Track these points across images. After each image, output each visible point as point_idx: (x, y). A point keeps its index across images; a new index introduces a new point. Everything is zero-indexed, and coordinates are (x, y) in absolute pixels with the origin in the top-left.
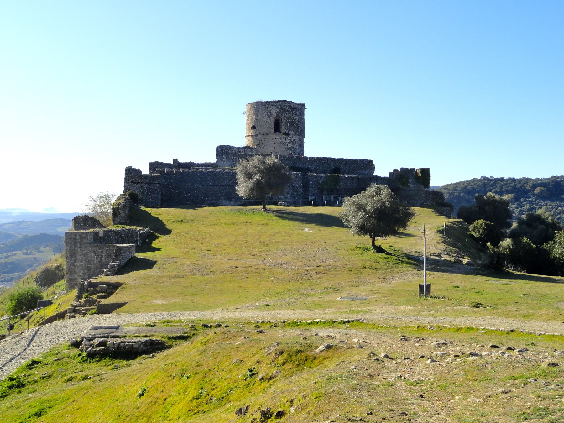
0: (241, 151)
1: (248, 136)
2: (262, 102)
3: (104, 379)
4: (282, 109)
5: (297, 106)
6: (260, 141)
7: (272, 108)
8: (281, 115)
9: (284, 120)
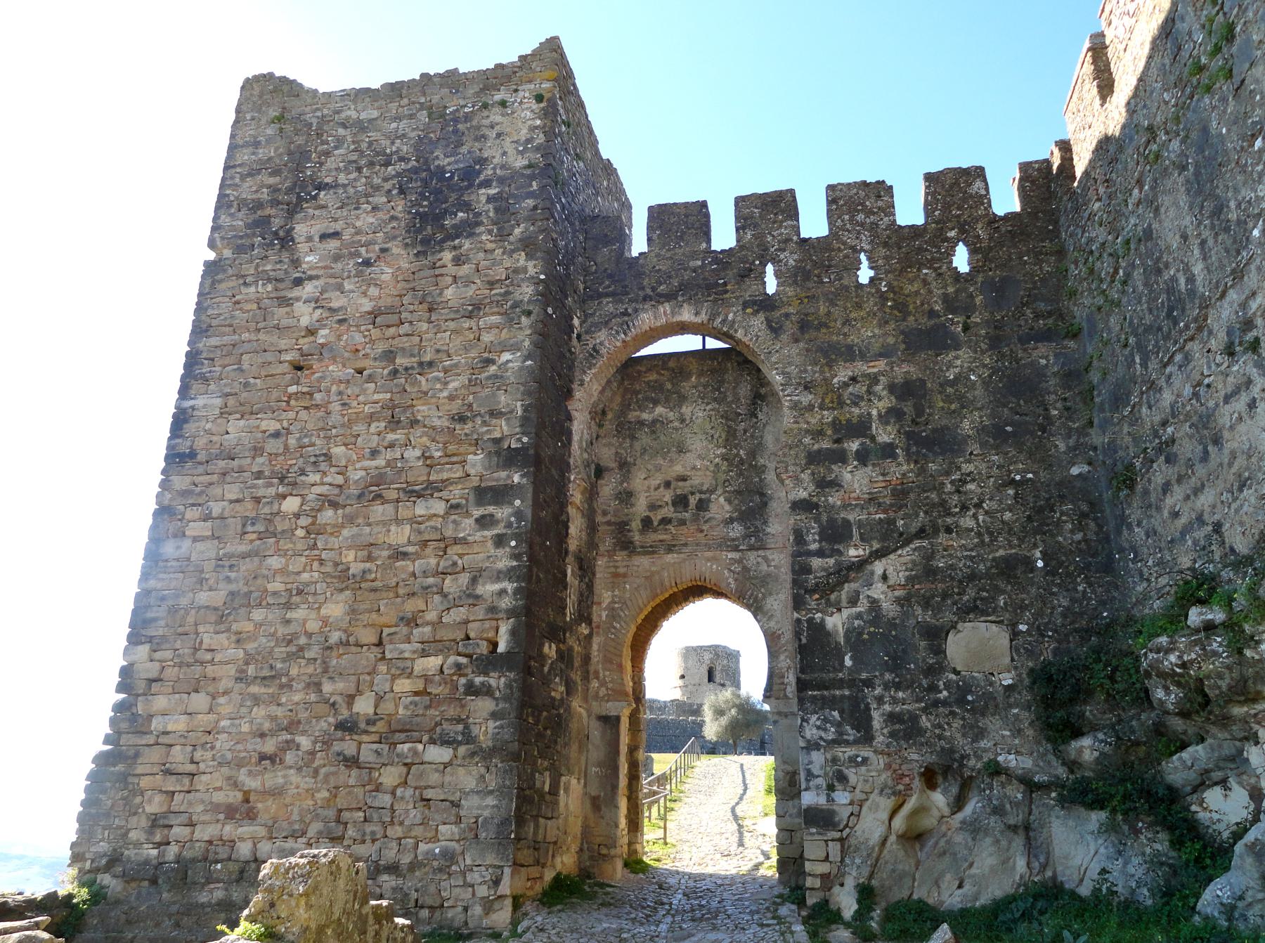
4: (717, 654)
6: (691, 693)
9: (719, 668)
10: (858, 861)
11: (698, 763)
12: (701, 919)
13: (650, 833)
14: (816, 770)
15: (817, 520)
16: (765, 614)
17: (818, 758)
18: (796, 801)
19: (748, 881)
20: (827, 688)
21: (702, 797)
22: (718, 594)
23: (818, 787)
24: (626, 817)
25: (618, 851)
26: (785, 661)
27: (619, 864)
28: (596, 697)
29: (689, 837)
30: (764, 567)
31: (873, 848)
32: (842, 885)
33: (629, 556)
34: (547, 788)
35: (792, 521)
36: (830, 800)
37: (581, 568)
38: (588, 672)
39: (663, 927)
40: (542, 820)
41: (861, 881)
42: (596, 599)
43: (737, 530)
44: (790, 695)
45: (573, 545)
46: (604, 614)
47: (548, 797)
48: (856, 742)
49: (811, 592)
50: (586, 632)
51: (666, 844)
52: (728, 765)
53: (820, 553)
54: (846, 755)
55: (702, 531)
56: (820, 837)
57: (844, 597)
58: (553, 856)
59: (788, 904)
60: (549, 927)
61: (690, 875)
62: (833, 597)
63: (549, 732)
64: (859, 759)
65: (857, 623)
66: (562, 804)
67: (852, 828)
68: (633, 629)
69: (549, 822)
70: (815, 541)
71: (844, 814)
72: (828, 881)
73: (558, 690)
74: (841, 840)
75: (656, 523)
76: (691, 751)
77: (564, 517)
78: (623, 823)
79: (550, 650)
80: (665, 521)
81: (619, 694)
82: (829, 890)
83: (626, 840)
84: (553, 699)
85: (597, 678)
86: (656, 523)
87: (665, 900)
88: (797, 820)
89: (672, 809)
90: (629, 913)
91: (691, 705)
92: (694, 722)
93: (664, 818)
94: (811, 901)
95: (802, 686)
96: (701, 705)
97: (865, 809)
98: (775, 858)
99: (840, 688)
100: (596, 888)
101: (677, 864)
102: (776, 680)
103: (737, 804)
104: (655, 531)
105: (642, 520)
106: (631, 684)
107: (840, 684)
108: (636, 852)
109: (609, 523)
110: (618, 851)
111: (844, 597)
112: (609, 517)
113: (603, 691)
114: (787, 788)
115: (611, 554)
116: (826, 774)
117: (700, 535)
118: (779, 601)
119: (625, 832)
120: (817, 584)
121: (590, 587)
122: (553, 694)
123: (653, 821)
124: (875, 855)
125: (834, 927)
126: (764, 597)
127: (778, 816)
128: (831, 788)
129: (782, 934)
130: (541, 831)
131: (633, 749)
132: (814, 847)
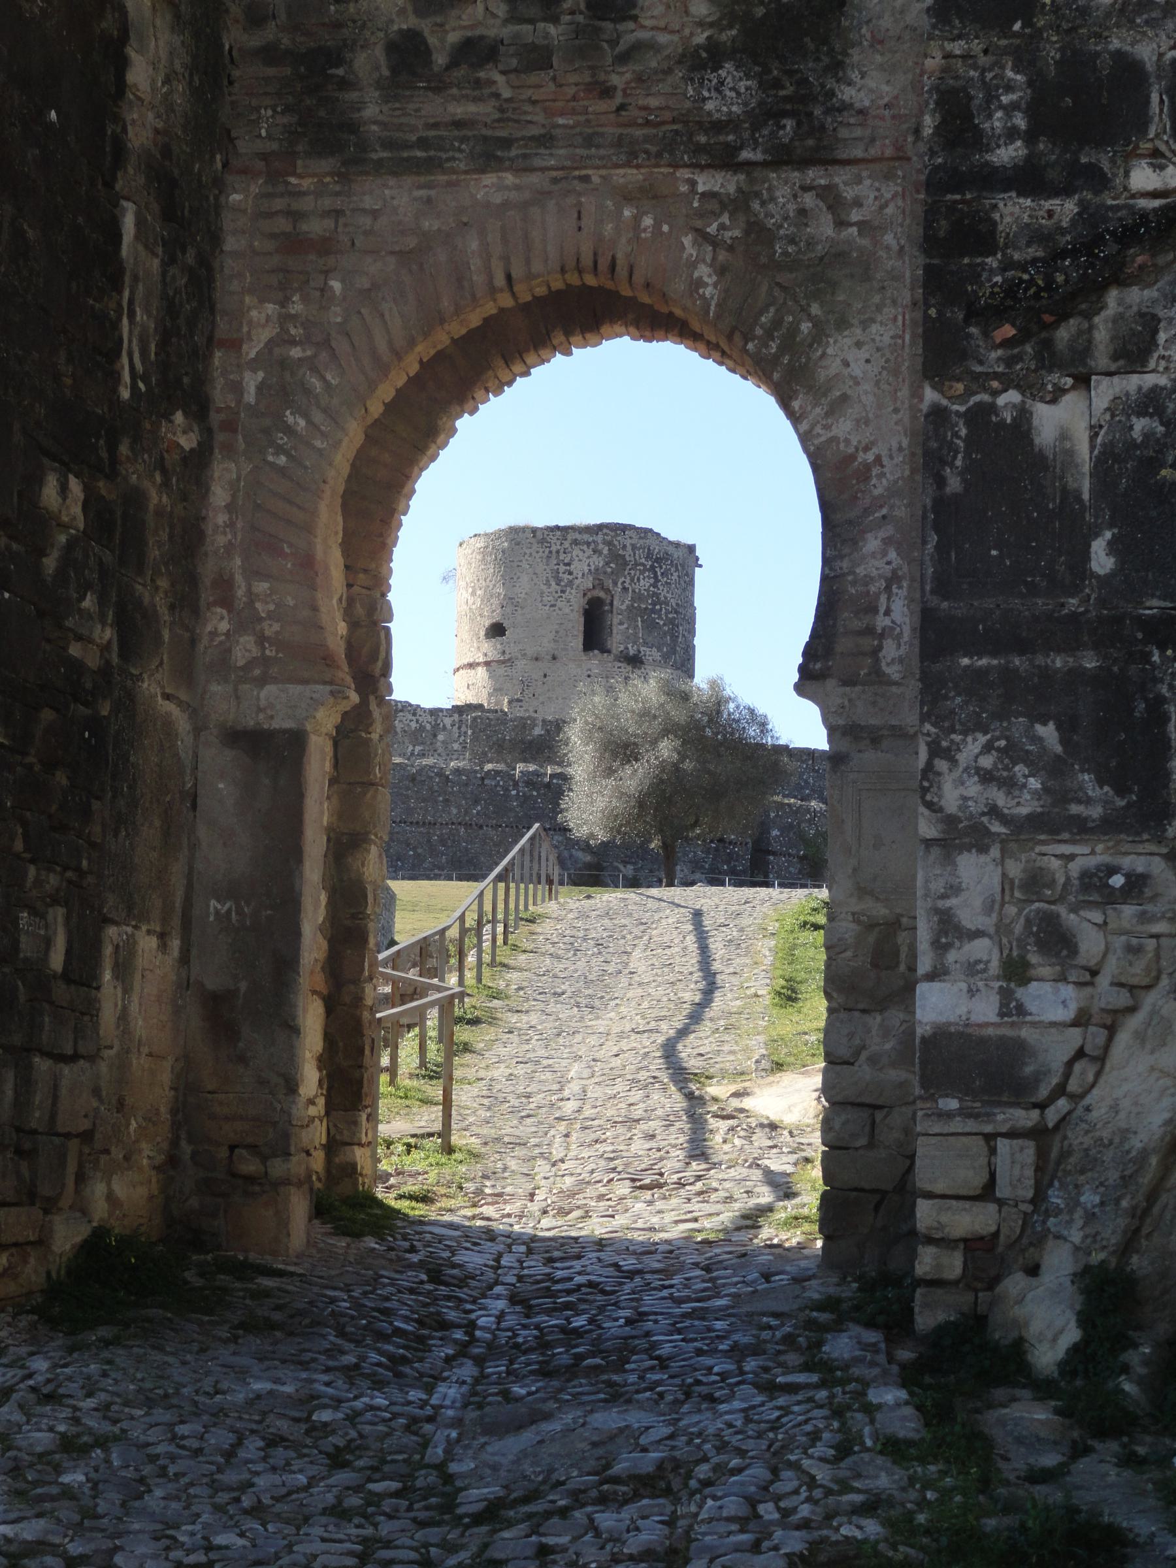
0: (448, 721)
1: (471, 666)
2: (534, 531)
3: (622, 1395)
4: (617, 558)
5: (671, 550)
6: (525, 684)
7: (576, 551)
8: (609, 583)
9: (621, 604)
10: (1089, 1198)
11: (552, 907)
12: (573, 1370)
13: (397, 1119)
14: (970, 913)
15: (1025, 58)
16: (818, 392)
17: (978, 875)
18: (895, 1016)
19: (715, 1272)
20: (1024, 647)
21: (565, 1012)
22: (655, 322)
23: (972, 968)
24: (323, 1062)
25: (295, 1165)
26: (877, 557)
27: (299, 1207)
28: (223, 665)
29: (526, 1129)
30: (824, 228)
31: (1144, 1154)
32: (1033, 1270)
33: (343, 177)
34: (57, 960)
35: (933, 63)
36: (1011, 1008)
37: (169, 214)
38: (193, 580)
39: (449, 1393)
40: (42, 1064)
41: (1097, 1257)
42: (223, 328)
43: (730, 93)
44: (893, 671)
45: (141, 128)
46: (251, 382)
47: (61, 992)
48: (1110, 826)
49: (987, 315)
50: (188, 442)
51: (449, 1149)
52: (656, 922)
53: (1028, 180)
54: (1075, 868)
55: (607, 92)
56: (971, 1126)
57: (1102, 335)
58: (81, 1178)
59: (856, 1329)
60: (73, 1388)
61: (531, 1243)
62: (1064, 334)
63: (61, 778)
64: (1117, 881)
65: (1140, 425)
66: (108, 1015)
67: (1076, 1098)
68: (353, 435)
69: (66, 1070)
70: (1012, 134)
71: (1056, 1051)
72: (987, 1259)
73: (95, 639)
74: (1039, 1134)
75: (440, 59)
76: (527, 873)
77: (108, 24)
78: (310, 1079)
79: (63, 498)
80: (476, 52)
81: (304, 659)
82: (996, 1280)
83: (318, 1134)
84: (77, 666)
85: (227, 602)
86: (440, 59)
87: (452, 1315)
88: (895, 1075)
89: (467, 1048)
90: (334, 1352)
91: (524, 725)
92: (531, 781)
93: (442, 1074)
94: (926, 1320)
95: (937, 637)
96: (557, 726)
97: (1123, 1038)
98: (810, 1200)
99: (1071, 647)
100: (223, 1279)
101: (489, 1211)
102: (848, 619)
103: (683, 1033)
104: (439, 86)
105: (392, 48)
106: (342, 628)
107: (1069, 633)
108: (351, 1170)
109: (269, 54)
110: (295, 1165)
111: (1102, 335)
112: (269, 33)
113: (244, 649)
114: (866, 978)
115: (276, 167)
116: (1002, 928)
117: (602, 106)
118: (869, 351)
119: (318, 1109)
120: (1011, 289)
121: (202, 280)
122: (75, 650)
123: (404, 1082)
124: (1146, 1179)
125: (1000, 1393)
126: (820, 333)
127: (832, 1060)
128: (1016, 972)
129: (838, 1413)
130: (39, 1097)
131: (345, 844)
132: (945, 1159)
